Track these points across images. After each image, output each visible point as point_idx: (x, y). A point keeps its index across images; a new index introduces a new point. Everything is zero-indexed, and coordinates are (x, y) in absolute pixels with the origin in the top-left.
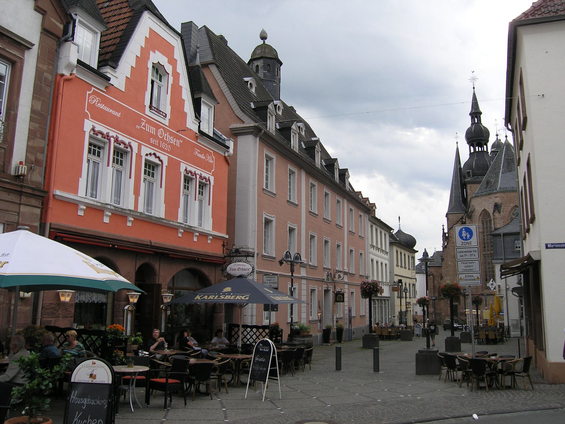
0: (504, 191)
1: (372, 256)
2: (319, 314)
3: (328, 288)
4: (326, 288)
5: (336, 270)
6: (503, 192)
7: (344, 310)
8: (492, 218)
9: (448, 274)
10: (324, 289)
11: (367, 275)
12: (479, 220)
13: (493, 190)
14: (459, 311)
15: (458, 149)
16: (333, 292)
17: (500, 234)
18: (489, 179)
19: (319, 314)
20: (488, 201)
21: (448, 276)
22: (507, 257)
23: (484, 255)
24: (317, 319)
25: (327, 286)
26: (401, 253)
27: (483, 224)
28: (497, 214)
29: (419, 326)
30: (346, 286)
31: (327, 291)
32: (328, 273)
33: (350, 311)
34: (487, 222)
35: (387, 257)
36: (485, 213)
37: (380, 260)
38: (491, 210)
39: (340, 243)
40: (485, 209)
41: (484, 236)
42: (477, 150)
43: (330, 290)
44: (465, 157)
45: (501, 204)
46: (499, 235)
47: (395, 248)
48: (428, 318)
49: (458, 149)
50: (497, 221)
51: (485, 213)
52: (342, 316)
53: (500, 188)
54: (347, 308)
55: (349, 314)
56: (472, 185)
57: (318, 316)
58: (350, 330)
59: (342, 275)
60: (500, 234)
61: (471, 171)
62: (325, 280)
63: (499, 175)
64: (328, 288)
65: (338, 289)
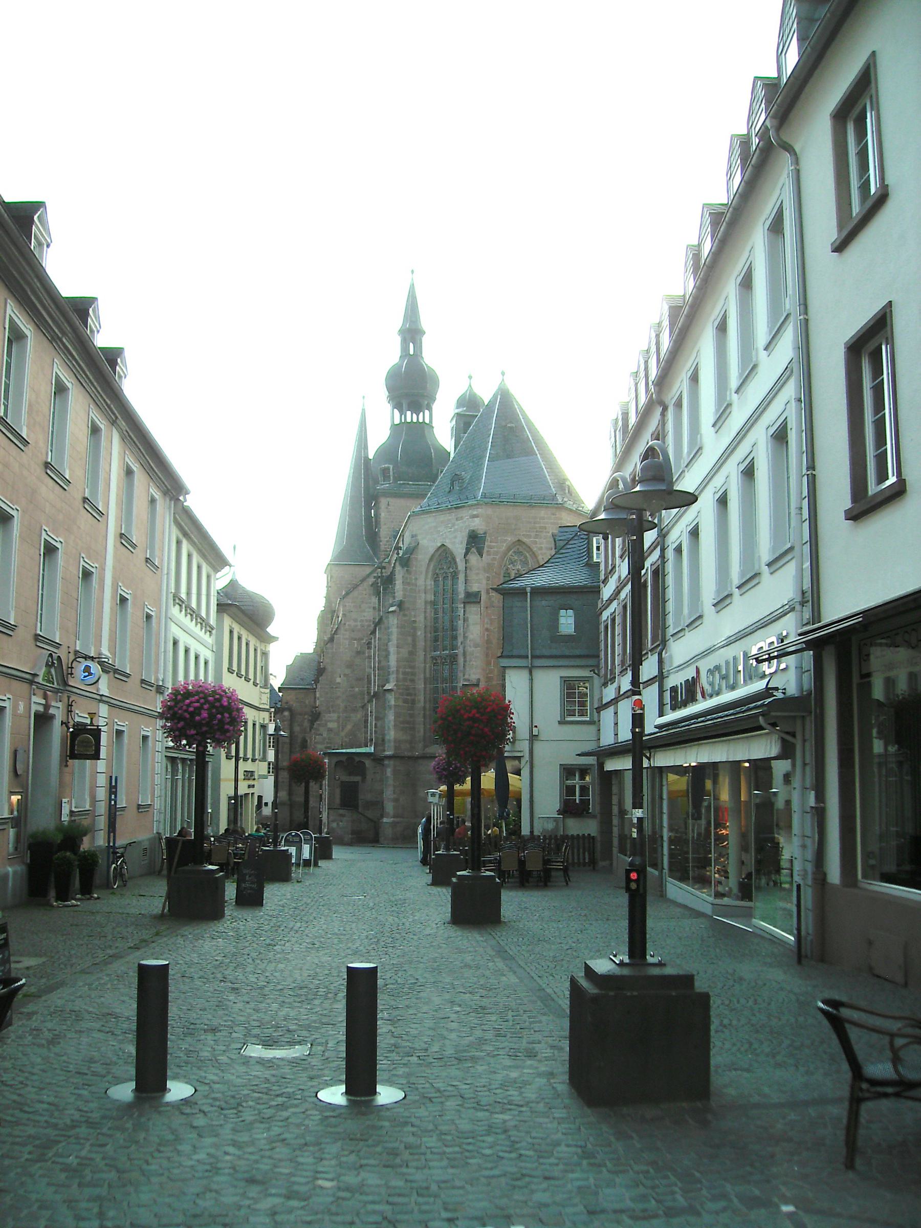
0: (493, 501)
1: (175, 631)
2: (15, 798)
3: (47, 707)
4: (41, 709)
5: (76, 652)
6: (492, 504)
7: (94, 787)
8: (461, 566)
9: (332, 706)
10: (34, 708)
11: (161, 684)
12: (427, 572)
13: (467, 498)
14: (361, 796)
15: (363, 410)
16: (62, 723)
17: (525, 589)
18: (458, 473)
19: (15, 798)
20: (454, 525)
21: (334, 712)
22: (538, 653)
23: (433, 658)
24: (6, 815)
25: (43, 702)
26: (239, 638)
27: (436, 580)
28: (474, 558)
29: (297, 839)
30: (104, 710)
31: (43, 719)
32: (51, 655)
33: (113, 790)
34: (445, 578)
35: (209, 640)
36: (443, 555)
37: (195, 647)
38: (458, 548)
39: (93, 566)
40: (443, 545)
41: (436, 613)
42: (409, 420)
43: (52, 717)
44: (378, 437)
45: (485, 533)
46: (521, 592)
47: (227, 622)
48: (637, 804)
49: (363, 410)
50: (472, 576)
51: (443, 555)
52: (88, 808)
53: (484, 496)
54: (102, 780)
55: (110, 800)
56: (392, 501)
57: (11, 804)
58: (112, 852)
59: (95, 668)
60: (525, 589)
61: (391, 467)
62: (40, 680)
63: (483, 464)
64: (47, 707)
65: (81, 716)
